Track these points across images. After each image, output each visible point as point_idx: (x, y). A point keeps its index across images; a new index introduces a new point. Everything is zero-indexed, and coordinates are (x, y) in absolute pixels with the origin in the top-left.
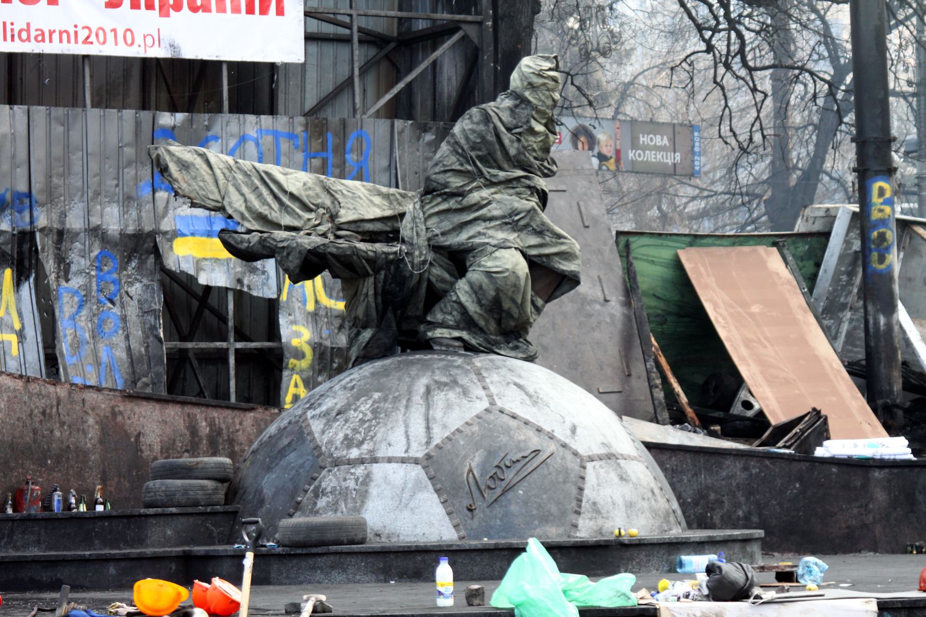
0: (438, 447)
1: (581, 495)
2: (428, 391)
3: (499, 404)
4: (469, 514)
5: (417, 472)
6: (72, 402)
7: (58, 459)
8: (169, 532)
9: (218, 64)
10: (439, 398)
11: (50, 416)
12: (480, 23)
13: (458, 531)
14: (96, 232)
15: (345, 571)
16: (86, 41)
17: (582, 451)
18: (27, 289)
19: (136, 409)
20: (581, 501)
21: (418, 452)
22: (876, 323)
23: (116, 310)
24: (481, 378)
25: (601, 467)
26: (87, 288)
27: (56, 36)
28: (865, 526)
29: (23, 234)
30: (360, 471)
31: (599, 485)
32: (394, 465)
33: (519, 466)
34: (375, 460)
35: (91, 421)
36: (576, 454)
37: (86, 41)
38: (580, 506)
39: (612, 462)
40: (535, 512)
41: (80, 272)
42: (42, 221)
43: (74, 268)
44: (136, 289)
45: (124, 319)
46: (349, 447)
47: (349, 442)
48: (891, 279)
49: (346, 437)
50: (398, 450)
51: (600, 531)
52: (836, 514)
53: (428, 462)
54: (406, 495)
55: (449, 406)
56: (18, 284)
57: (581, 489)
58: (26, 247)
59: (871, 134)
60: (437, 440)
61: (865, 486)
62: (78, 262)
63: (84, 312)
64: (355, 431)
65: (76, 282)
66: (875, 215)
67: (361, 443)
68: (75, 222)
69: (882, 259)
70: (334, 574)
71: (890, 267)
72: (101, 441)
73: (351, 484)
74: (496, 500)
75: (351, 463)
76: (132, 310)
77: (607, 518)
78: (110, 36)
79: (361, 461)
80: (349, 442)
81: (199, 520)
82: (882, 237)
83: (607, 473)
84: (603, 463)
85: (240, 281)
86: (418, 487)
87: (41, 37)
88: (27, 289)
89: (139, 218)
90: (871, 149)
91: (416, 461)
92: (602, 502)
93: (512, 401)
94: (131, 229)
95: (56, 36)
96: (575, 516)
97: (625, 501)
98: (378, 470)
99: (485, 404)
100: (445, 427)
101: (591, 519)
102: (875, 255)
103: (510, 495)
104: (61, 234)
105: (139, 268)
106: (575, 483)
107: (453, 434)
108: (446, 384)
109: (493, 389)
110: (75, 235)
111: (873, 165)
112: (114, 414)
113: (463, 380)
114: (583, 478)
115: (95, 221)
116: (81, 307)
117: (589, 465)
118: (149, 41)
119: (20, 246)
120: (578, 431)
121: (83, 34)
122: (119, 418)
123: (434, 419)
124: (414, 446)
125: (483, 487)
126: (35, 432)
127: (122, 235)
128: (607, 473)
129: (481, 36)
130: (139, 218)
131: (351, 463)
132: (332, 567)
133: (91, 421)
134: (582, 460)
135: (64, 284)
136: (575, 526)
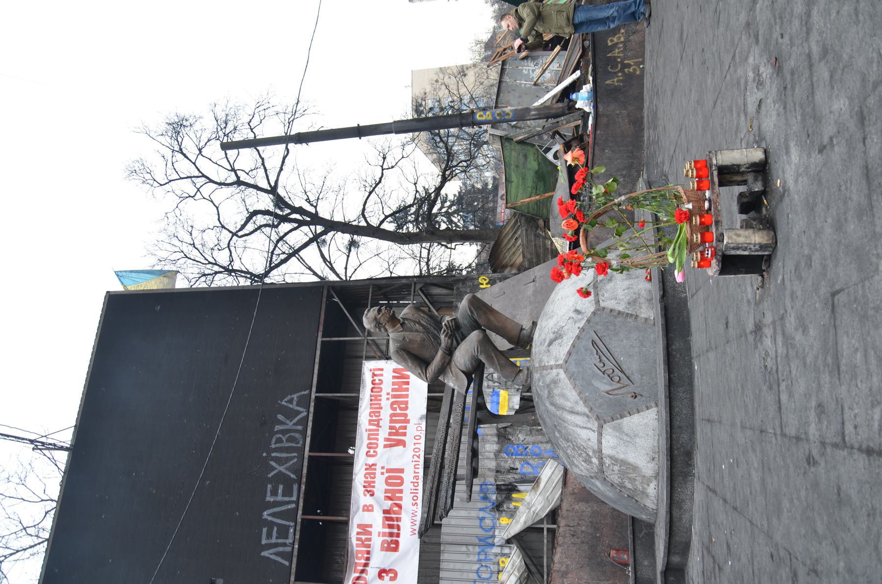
0: (591, 410)
1: (623, 313)
2: (552, 404)
3: (561, 362)
4: (639, 397)
5: (608, 429)
6: (568, 517)
7: (597, 529)
8: (646, 563)
9: (429, 398)
10: (560, 401)
11: (575, 531)
12: (415, 284)
13: (651, 407)
14: (497, 454)
15: (683, 501)
16: (419, 457)
17: (592, 309)
18: (521, 487)
19: (571, 481)
20: (628, 314)
21: (595, 425)
22: (534, 115)
23: (530, 446)
24: (545, 368)
25: (603, 295)
26: (521, 460)
27: (417, 470)
28: (629, 115)
29: (497, 489)
30: (607, 461)
31: (616, 299)
32: (603, 441)
33: (604, 358)
34: (600, 451)
35: (577, 507)
36: (594, 313)
37: (419, 457)
38: (632, 315)
39: (599, 286)
40: (637, 350)
41: (514, 463)
42: (491, 480)
43: (512, 466)
44: (521, 437)
45: (534, 443)
46: (591, 462)
47: (588, 460)
48: (516, 110)
49: (585, 461)
50: (594, 436)
51: (650, 300)
52: (482, 60)
53: (602, 422)
54: (625, 438)
55: (563, 396)
56: (519, 491)
57: (619, 312)
58: (503, 487)
59: (458, 121)
60: (586, 410)
61: (607, 116)
62: (509, 464)
63: (531, 462)
64: (580, 455)
65: (518, 465)
66: (490, 118)
67: (588, 455)
68: (492, 464)
69: (508, 114)
70: (686, 507)
71: (511, 111)
72: (588, 502)
73: (616, 468)
74: (628, 378)
75: (602, 463)
76: (530, 439)
77: (639, 294)
78: (417, 446)
79: (601, 459)
80: (588, 460)
81: (638, 542)
82: (499, 115)
83: (607, 291)
84: (600, 294)
85: (518, 390)
86: (619, 429)
87: (416, 477)
88: (521, 487)
89: (491, 435)
90: (464, 121)
91: (601, 427)
92: (628, 298)
93: (561, 351)
94: (496, 439)
95: (417, 470)
96: (639, 319)
97: (626, 279)
98: (606, 451)
99: (561, 371)
100: (577, 403)
101: (641, 307)
102: (507, 117)
103: (624, 367)
104: (497, 471)
105: (513, 435)
106: (615, 317)
107: (581, 398)
108: (549, 392)
109: (552, 363)
110: (498, 465)
111: (471, 119)
112: (574, 494)
113: (548, 380)
114: (611, 310)
115: (492, 455)
116: (528, 464)
117: (602, 304)
118: (419, 429)
119: (502, 490)
120: (579, 308)
121: (416, 458)
122: (576, 491)
123: (571, 408)
124: (589, 425)
125: (619, 385)
126: (583, 542)
127: (498, 443)
128: (607, 291)
129: (420, 283)
130: (491, 435)
131: (602, 463)
132: (681, 508)
133: (577, 507)
134: (599, 310)
135: (518, 471)
136: (646, 319)
